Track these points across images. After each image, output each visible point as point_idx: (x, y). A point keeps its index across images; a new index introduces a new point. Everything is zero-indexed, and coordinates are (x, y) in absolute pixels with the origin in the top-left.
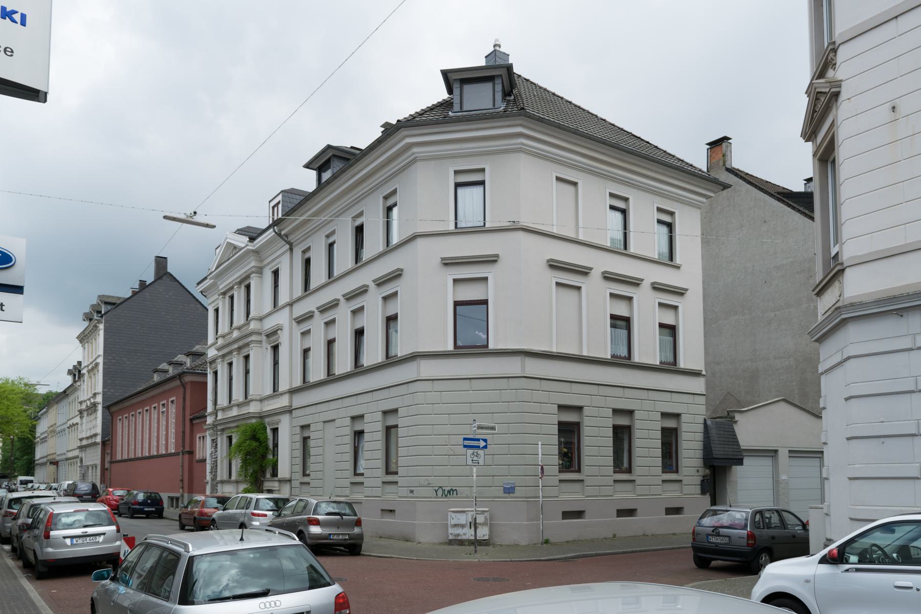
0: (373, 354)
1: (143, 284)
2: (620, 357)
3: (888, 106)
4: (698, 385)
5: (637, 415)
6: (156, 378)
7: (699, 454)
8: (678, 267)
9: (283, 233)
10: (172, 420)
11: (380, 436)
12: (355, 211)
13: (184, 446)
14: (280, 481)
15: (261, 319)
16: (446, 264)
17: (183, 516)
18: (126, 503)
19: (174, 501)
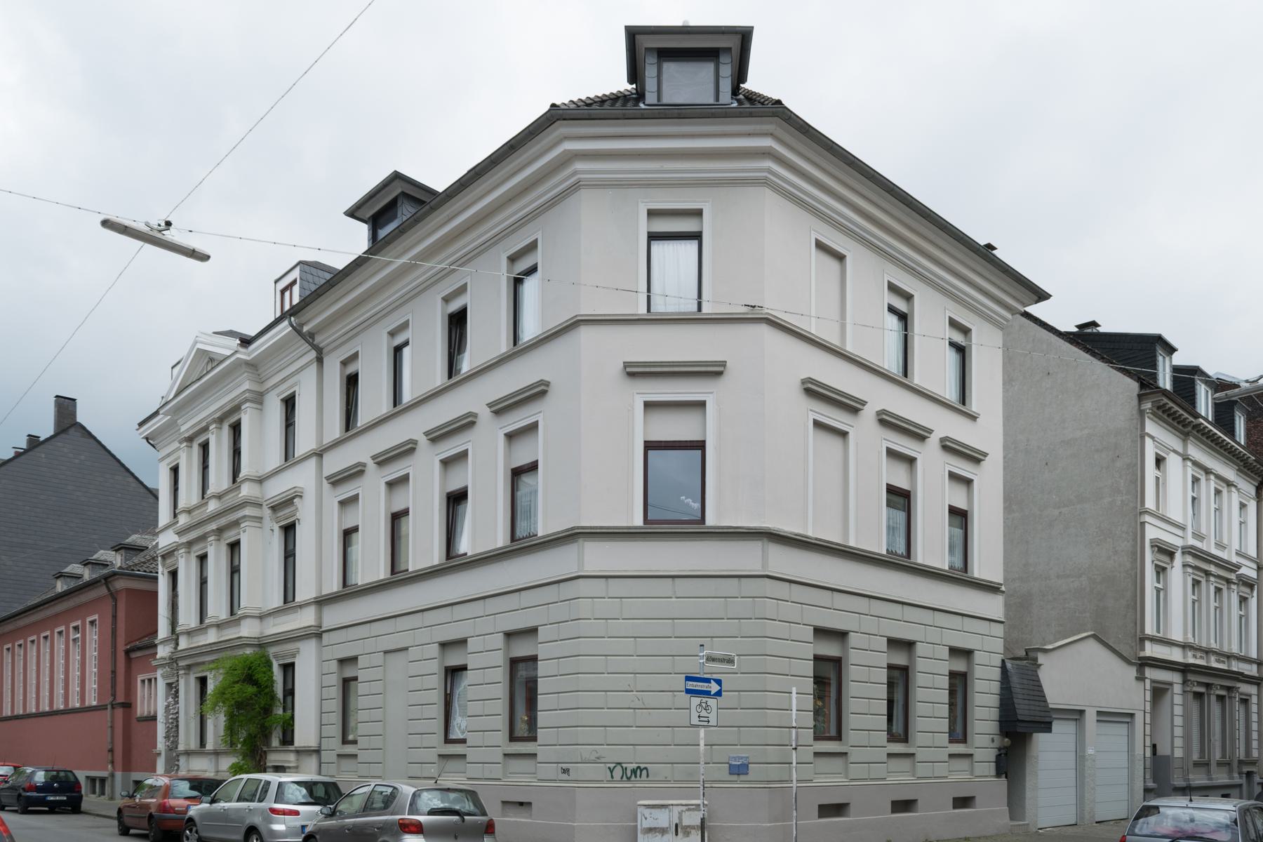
1: (34, 441)
2: (896, 554)
4: (993, 606)
6: (60, 587)
8: (973, 418)
9: (305, 329)
10: (92, 653)
13: (114, 695)
14: (298, 752)
15: (260, 481)
16: (632, 375)
17: (126, 813)
18: (12, 788)
19: (98, 784)
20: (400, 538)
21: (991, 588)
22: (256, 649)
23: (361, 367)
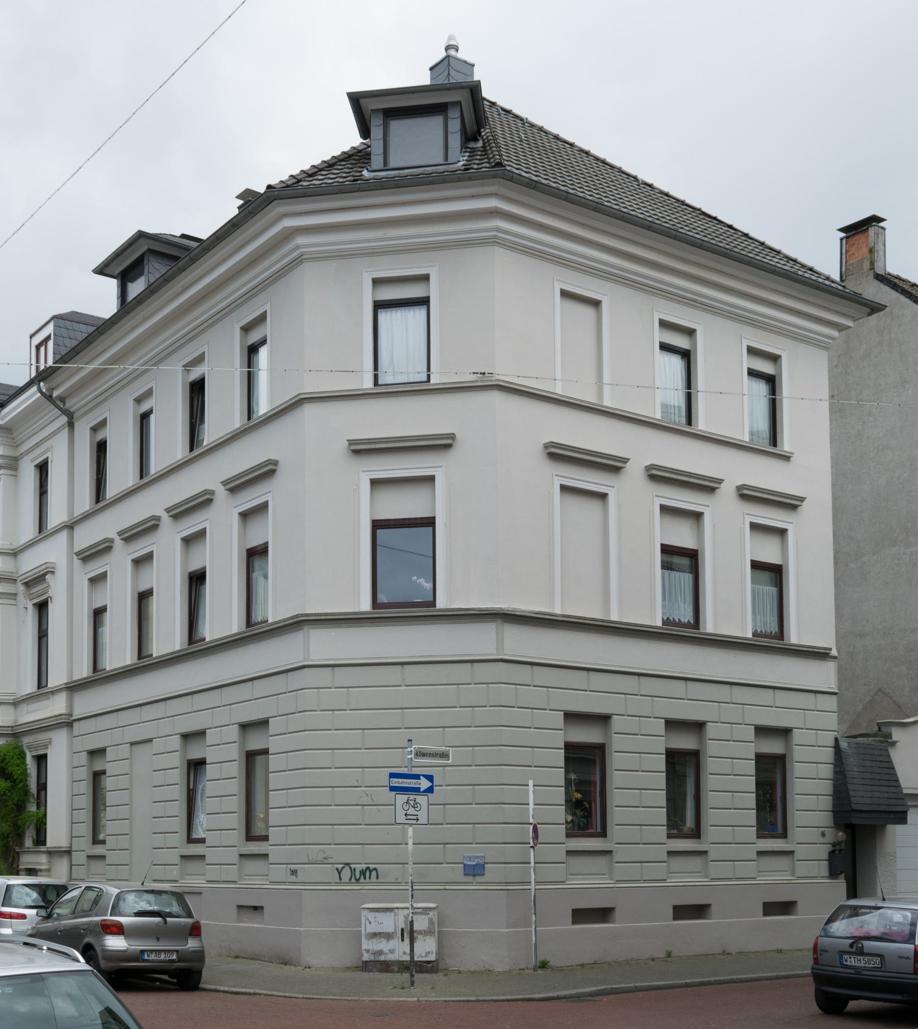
0: (222, 616)
2: (680, 624)
4: (823, 675)
7: (826, 803)
8: (786, 458)
11: (235, 769)
12: (189, 354)
14: (50, 853)
16: (357, 452)
20: (147, 618)
21: (820, 655)
22: (10, 739)
23: (108, 433)
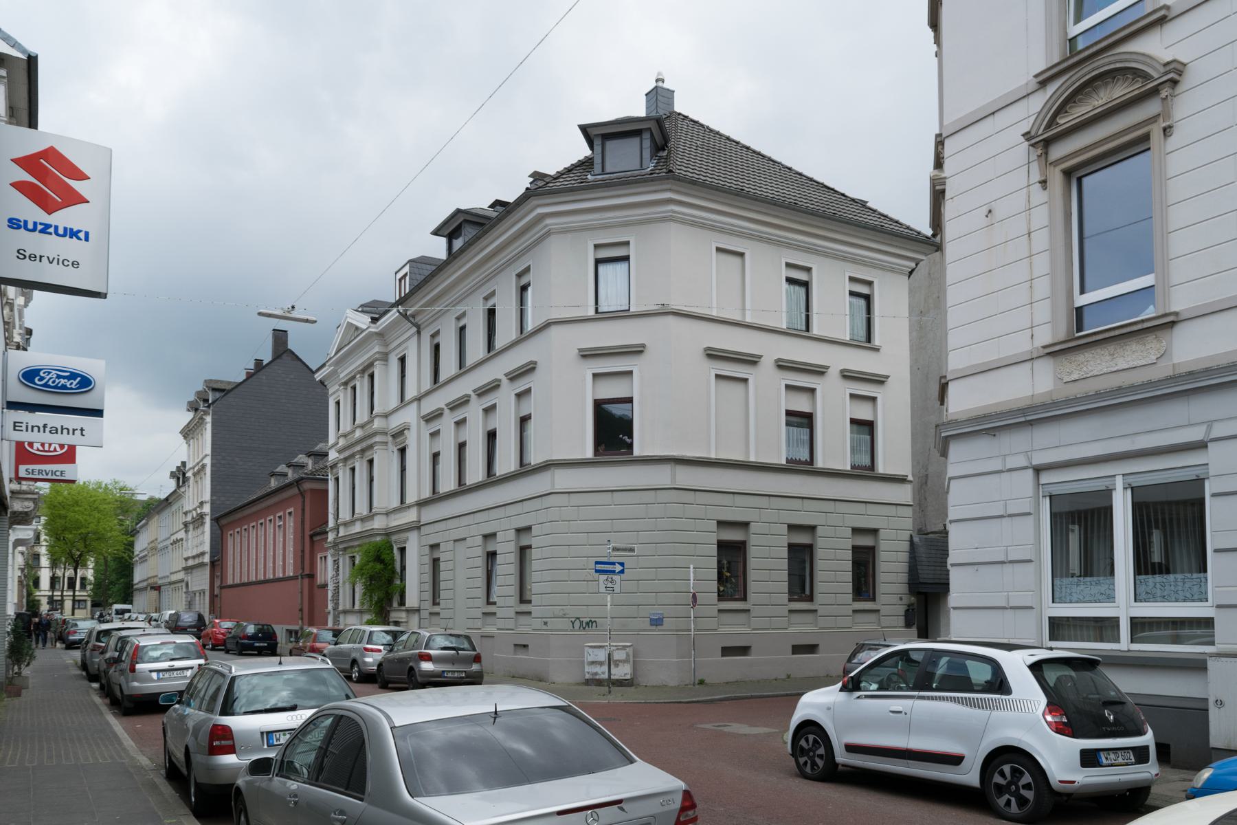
0: (506, 462)
1: (258, 362)
3: (984, 210)
4: (904, 494)
5: (820, 531)
6: (274, 483)
7: (904, 578)
8: (877, 350)
10: (290, 536)
11: (513, 558)
12: (460, 309)
13: (303, 569)
14: (408, 611)
15: (386, 416)
16: (584, 356)
18: (234, 637)
21: (901, 480)
